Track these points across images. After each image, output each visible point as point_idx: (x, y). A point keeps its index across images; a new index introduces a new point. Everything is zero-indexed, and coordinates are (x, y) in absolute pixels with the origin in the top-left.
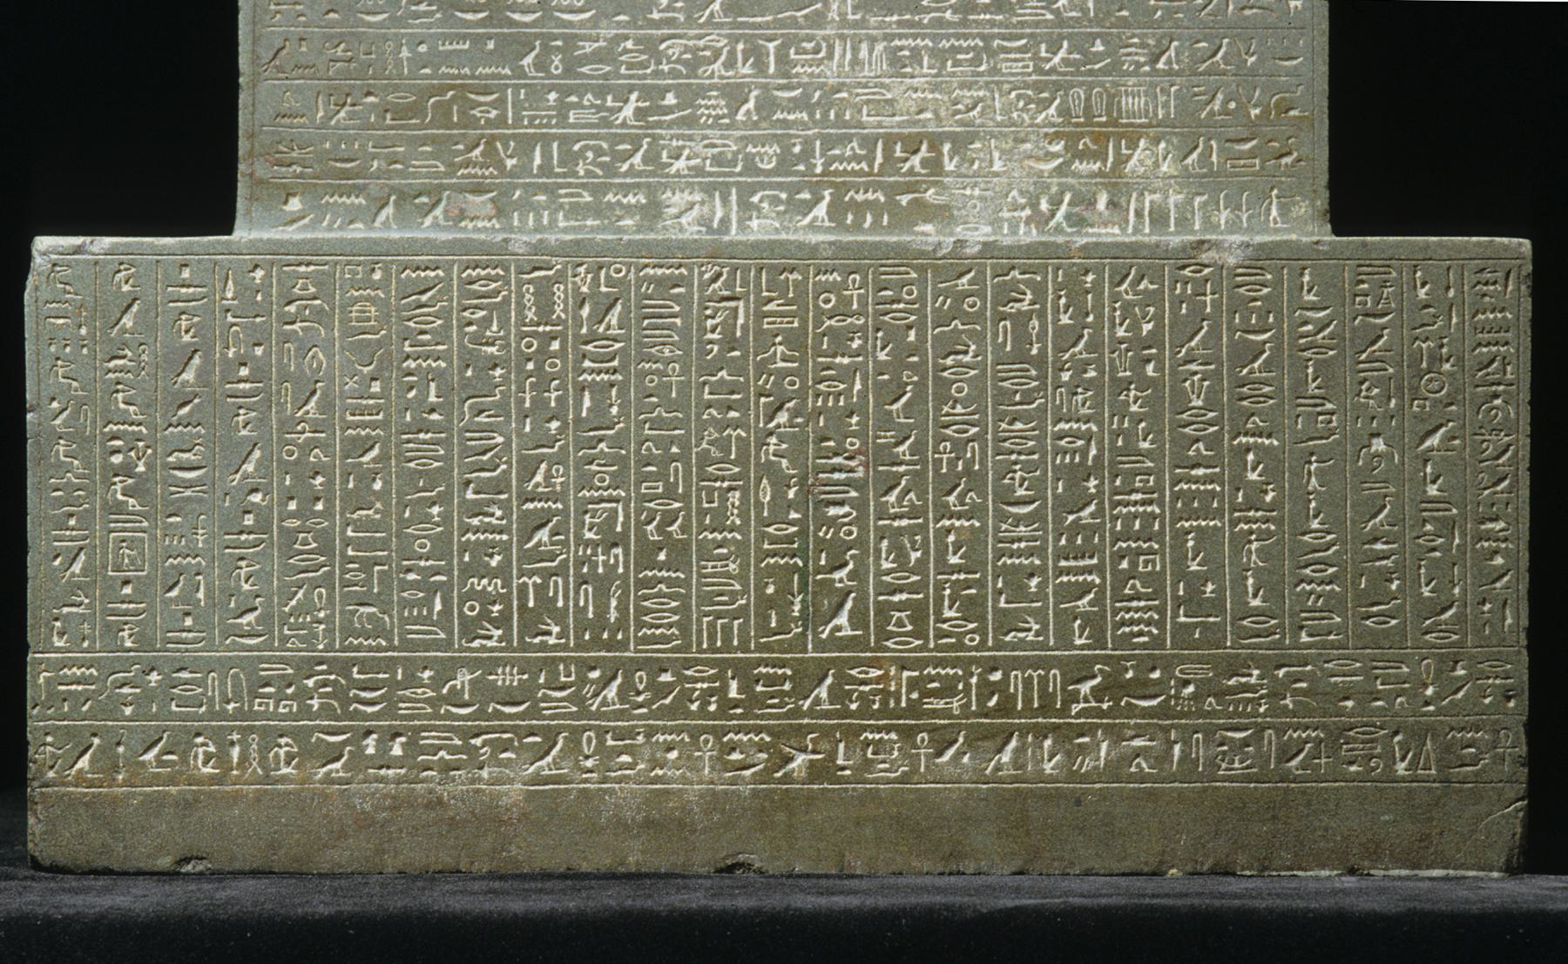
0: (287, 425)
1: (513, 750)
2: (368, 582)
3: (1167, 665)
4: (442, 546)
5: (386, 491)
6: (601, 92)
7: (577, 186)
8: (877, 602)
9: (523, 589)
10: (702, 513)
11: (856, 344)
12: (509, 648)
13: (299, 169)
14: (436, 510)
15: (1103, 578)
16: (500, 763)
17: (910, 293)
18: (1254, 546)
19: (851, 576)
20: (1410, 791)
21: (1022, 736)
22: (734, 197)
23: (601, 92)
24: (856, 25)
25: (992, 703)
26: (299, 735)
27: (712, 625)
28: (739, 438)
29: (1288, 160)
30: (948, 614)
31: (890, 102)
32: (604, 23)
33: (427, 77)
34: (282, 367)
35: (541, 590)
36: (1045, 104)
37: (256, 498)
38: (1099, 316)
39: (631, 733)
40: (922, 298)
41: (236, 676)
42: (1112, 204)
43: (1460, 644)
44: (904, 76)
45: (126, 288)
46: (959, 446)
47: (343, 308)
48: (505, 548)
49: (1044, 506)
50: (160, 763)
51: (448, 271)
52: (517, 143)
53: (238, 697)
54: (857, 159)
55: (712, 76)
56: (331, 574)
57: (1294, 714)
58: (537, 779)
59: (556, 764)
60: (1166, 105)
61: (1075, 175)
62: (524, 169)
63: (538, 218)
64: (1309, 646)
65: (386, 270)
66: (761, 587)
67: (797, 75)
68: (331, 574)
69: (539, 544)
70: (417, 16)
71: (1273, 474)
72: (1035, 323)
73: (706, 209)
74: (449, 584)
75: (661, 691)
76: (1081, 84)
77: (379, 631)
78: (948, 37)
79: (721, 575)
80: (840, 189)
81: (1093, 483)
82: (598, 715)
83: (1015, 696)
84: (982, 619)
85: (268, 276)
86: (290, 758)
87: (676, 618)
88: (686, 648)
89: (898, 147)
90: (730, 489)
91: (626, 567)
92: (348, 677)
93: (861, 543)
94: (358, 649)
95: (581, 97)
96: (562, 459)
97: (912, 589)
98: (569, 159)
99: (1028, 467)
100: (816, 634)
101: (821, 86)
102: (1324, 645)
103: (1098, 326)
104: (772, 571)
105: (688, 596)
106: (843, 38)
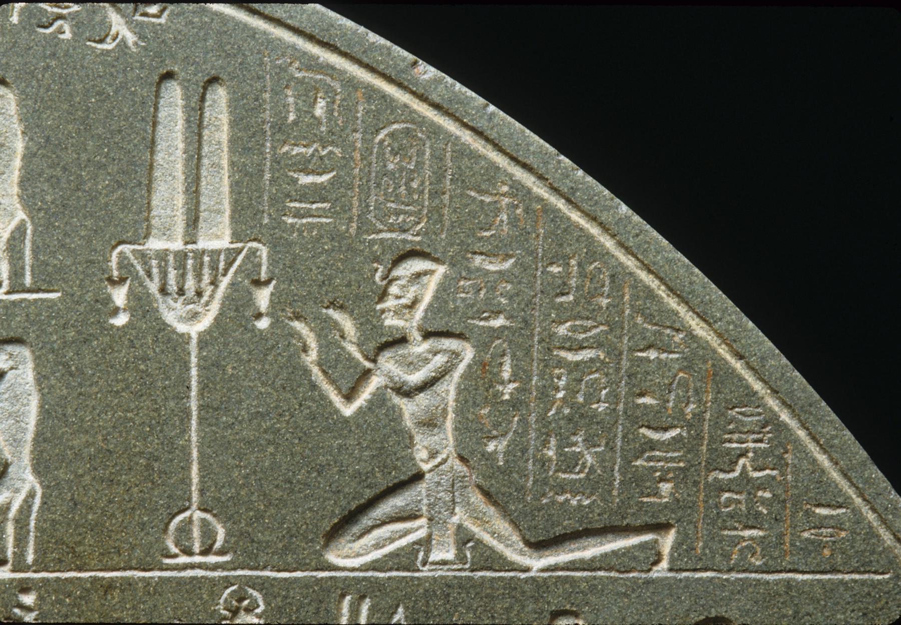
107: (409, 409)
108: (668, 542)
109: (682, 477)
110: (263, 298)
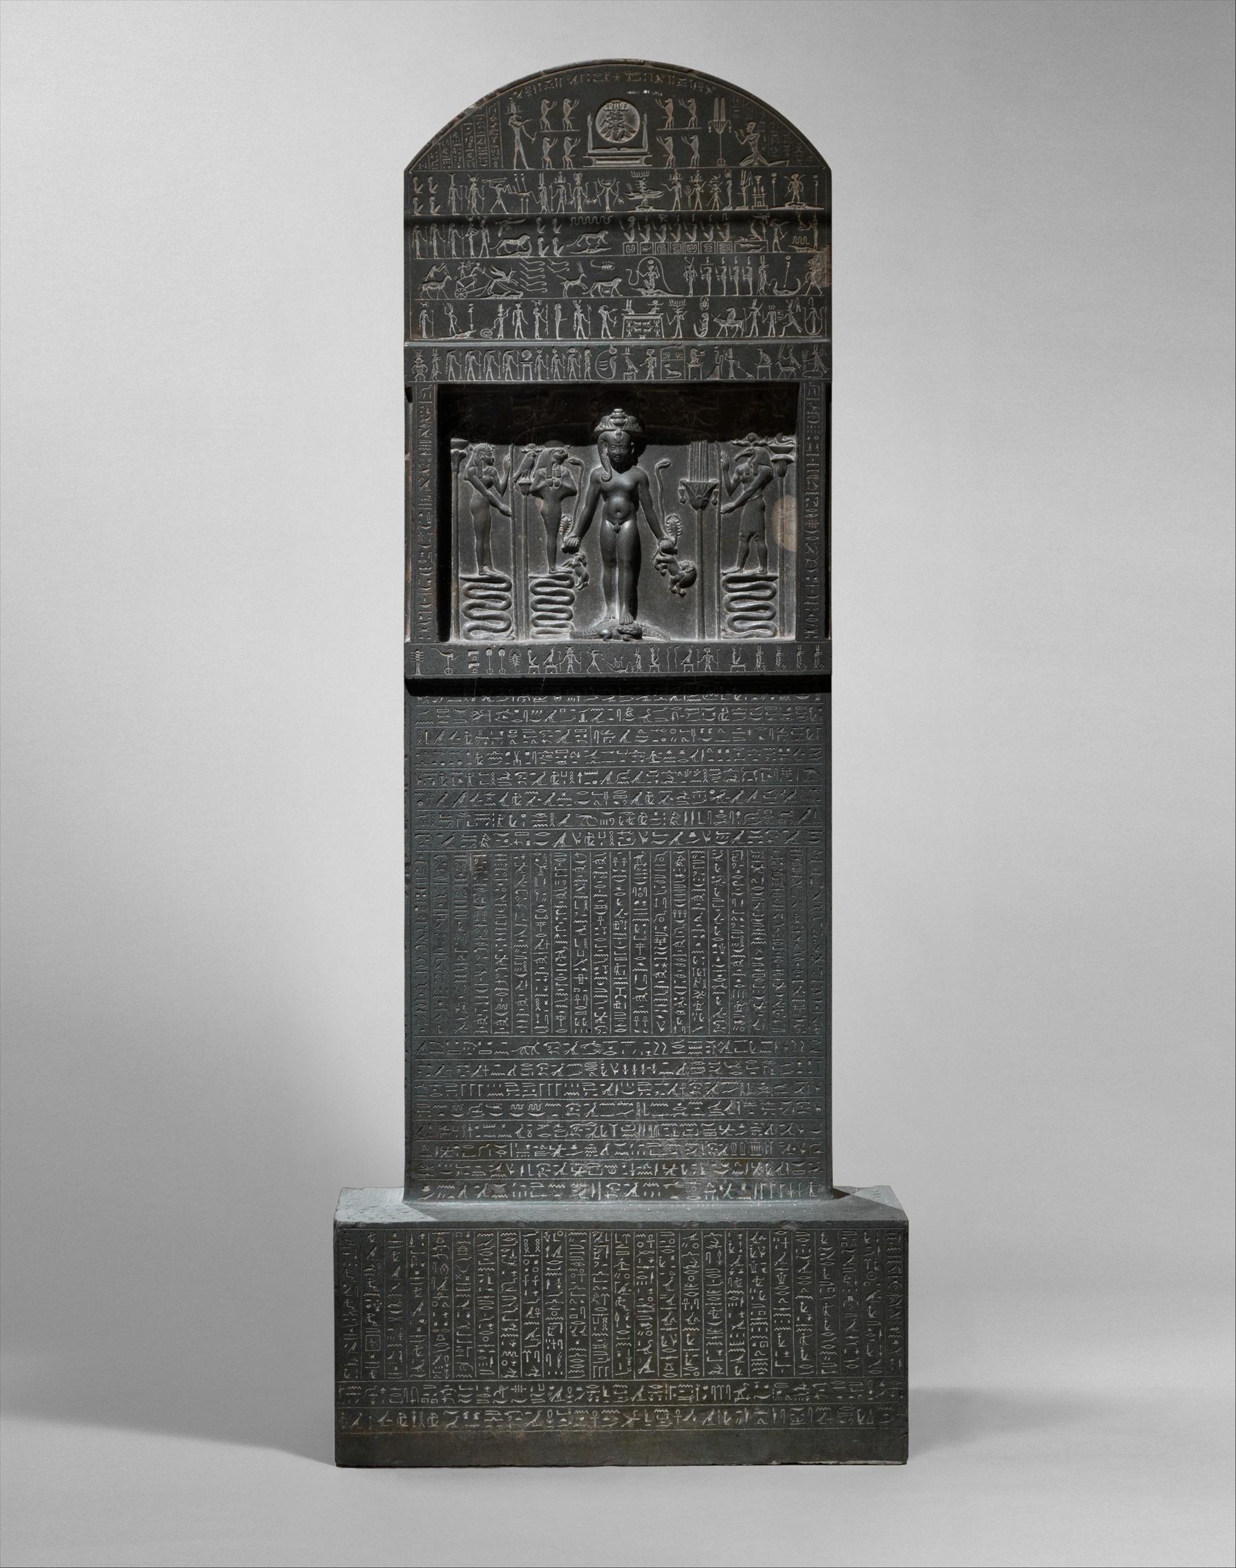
0: (434, 1293)
1: (521, 1417)
2: (464, 1353)
3: (771, 1383)
4: (493, 1339)
5: (471, 1319)
6: (547, 1144)
7: (538, 1181)
8: (660, 1360)
9: (524, 1355)
10: (593, 1326)
11: (651, 1261)
12: (519, 1378)
13: (428, 1175)
14: (491, 1325)
15: (747, 1350)
16: (516, 1422)
17: (672, 1241)
18: (804, 1337)
19: (650, 1350)
20: (864, 1430)
21: (716, 1410)
22: (599, 1186)
23: (547, 1144)
24: (647, 1118)
25: (705, 1398)
26: (439, 1412)
27: (597, 1369)
28: (607, 1297)
29: (816, 1170)
30: (687, 1364)
31: (661, 1148)
32: (548, 1117)
33: (478, 1138)
34: (432, 1271)
35: (531, 1356)
36: (721, 1149)
37: (422, 1321)
38: (744, 1243)
39: (566, 1410)
40: (676, 1244)
41: (414, 1390)
42: (747, 1188)
43: (882, 1374)
44: (667, 1137)
45: (372, 1241)
46: (691, 1300)
47: (455, 1248)
48: (517, 1340)
49: (724, 1322)
50: (385, 1423)
51: (495, 1235)
52: (515, 1164)
53: (415, 1397)
54: (648, 1170)
55: (591, 1138)
56: (451, 1350)
57: (820, 1401)
58: (530, 1428)
59: (537, 1422)
60: (769, 1149)
61: (734, 1176)
62: (517, 1174)
63: (523, 1194)
64: (825, 1375)
65: (472, 1234)
66: (615, 1354)
67: (624, 1137)
68: (451, 1350)
69: (530, 1338)
70: (475, 1114)
71: (810, 1310)
72: (720, 1252)
73: (589, 1190)
74: (496, 1353)
75: (576, 1394)
76: (735, 1141)
77: (469, 1371)
78: (683, 1122)
79: (601, 1350)
80: (641, 1182)
81: (742, 1314)
82: (554, 1403)
83: (713, 1395)
84: (700, 1366)
85: (426, 1236)
86: (435, 1420)
87: (583, 1366)
88: (587, 1377)
89: (664, 1166)
90: (603, 1317)
91: (564, 1347)
92: (457, 1389)
93: (653, 1337)
94: (462, 1378)
95: (539, 1146)
96: (539, 1305)
97: (673, 1354)
98: (535, 1171)
99: (717, 1308)
100: (637, 1372)
101: (634, 1142)
102: (831, 1375)
103: (743, 1254)
104: (620, 1348)
105: (588, 1358)
106: (642, 1123)
107: (751, 143)
108: (788, 162)
109: (790, 153)
110: (730, 128)
